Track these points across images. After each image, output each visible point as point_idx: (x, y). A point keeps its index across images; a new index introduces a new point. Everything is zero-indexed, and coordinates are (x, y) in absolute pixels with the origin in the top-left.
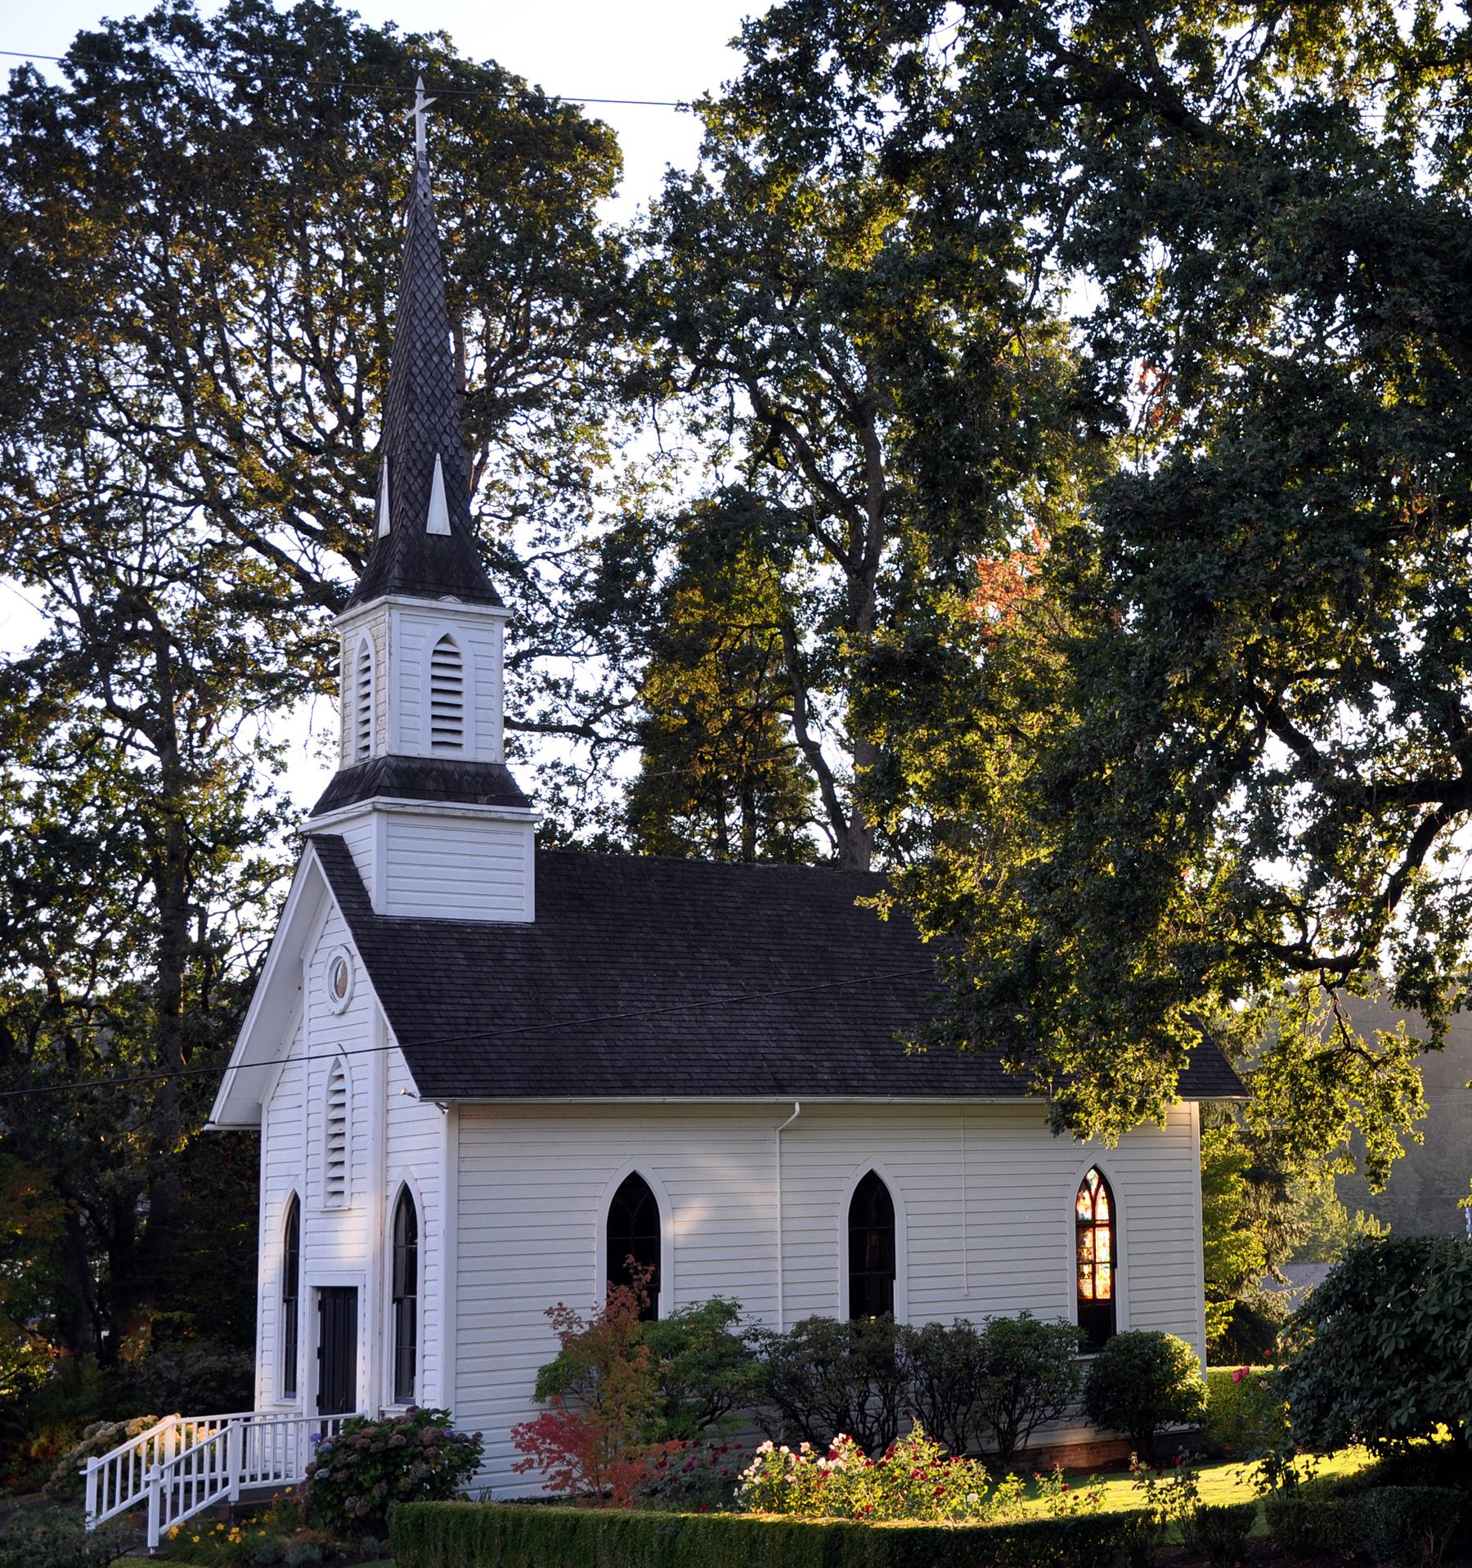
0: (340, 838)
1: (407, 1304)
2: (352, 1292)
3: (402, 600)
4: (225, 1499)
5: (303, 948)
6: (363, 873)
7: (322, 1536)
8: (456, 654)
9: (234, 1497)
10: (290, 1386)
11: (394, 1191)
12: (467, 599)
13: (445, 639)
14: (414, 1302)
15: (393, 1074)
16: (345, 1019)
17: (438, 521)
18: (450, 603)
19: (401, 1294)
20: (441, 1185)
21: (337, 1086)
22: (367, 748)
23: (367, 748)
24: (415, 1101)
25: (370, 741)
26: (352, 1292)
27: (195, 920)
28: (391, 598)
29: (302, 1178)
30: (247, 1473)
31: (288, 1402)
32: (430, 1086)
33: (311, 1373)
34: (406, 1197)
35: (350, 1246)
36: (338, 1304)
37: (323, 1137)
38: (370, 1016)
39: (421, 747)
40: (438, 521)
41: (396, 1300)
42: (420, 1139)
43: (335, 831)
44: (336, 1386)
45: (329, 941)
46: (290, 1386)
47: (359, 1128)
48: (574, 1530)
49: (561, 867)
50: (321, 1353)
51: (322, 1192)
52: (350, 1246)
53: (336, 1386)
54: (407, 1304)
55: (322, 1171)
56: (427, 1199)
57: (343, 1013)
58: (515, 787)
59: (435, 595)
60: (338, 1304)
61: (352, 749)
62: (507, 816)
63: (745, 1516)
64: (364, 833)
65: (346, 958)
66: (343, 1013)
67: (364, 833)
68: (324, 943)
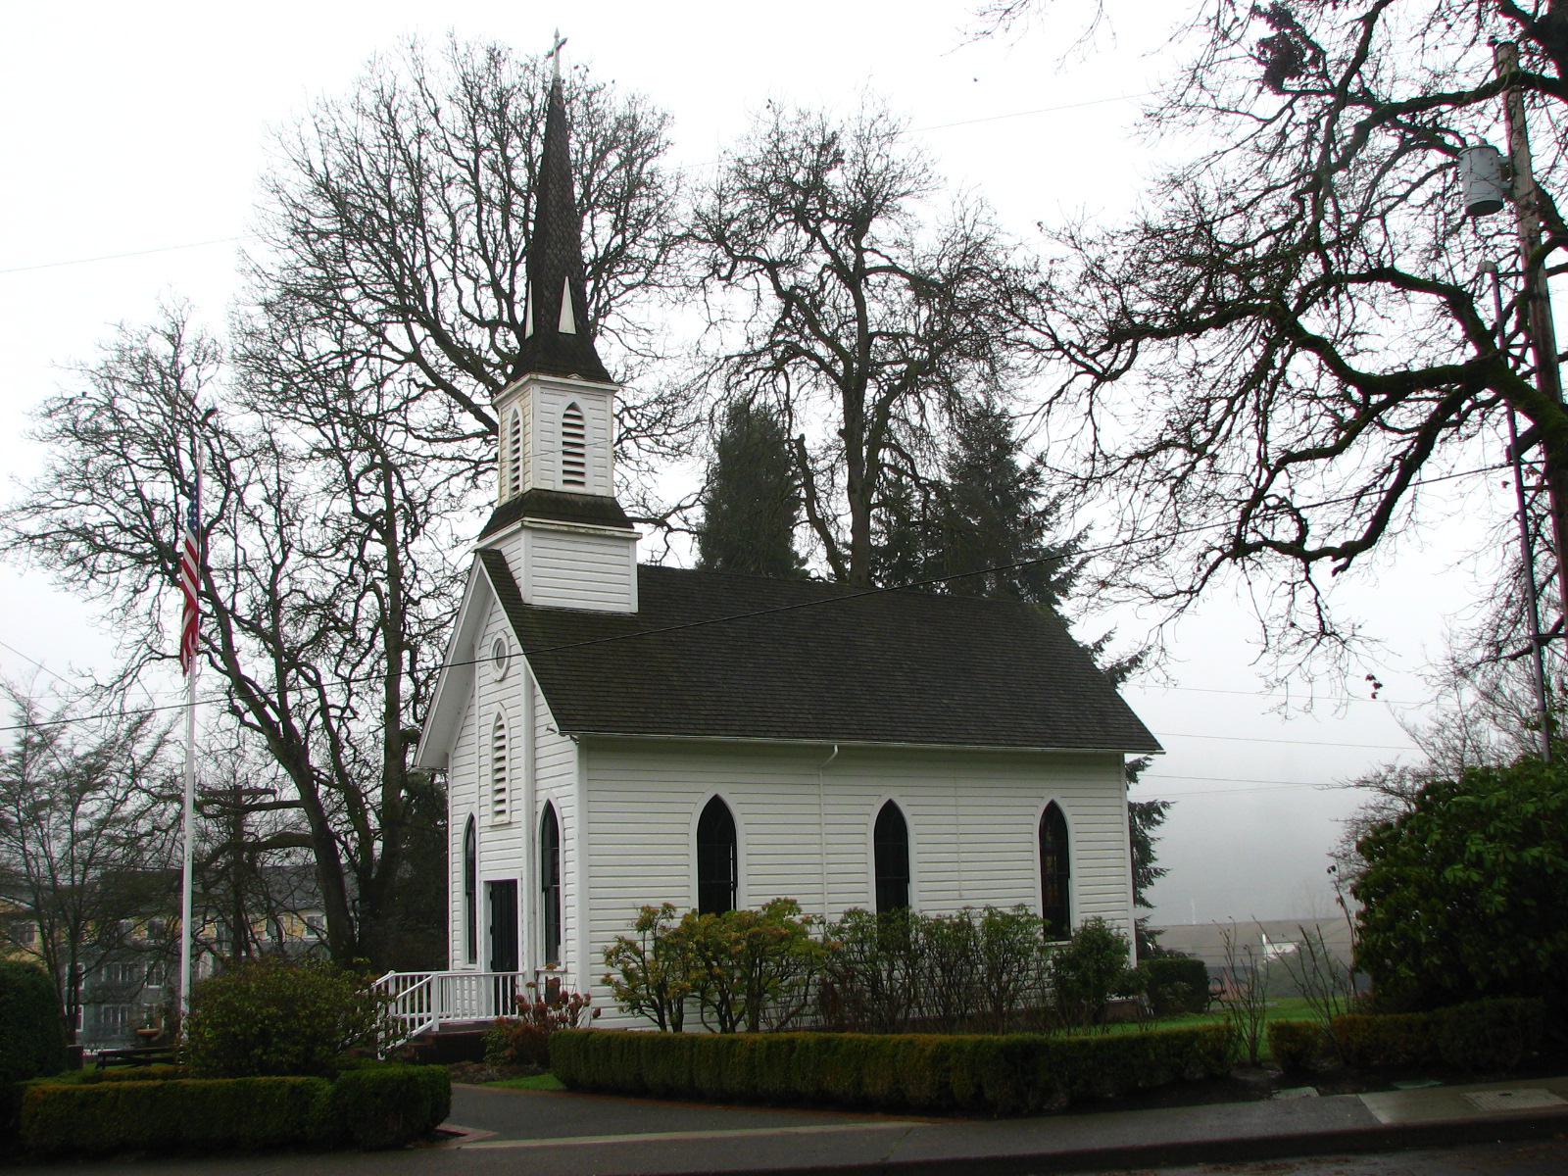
0: (499, 552)
1: (552, 891)
2: (514, 883)
3: (542, 377)
4: (430, 1028)
5: (472, 649)
6: (515, 575)
7: (1147, 831)
8: (579, 418)
9: (436, 1029)
10: (472, 956)
11: (541, 808)
12: (588, 378)
13: (572, 406)
14: (557, 890)
15: (540, 721)
16: (507, 683)
17: (567, 324)
18: (575, 380)
19: (547, 885)
20: (574, 800)
21: (500, 733)
22: (517, 487)
23: (517, 487)
24: (556, 737)
25: (520, 482)
26: (514, 883)
27: (406, 654)
28: (534, 376)
29: (476, 806)
30: (444, 1014)
31: (472, 966)
32: (566, 723)
33: (486, 945)
34: (549, 810)
35: (506, 856)
36: (504, 894)
37: (490, 782)
38: (521, 679)
39: (554, 482)
40: (567, 324)
41: (544, 889)
42: (557, 766)
43: (497, 548)
44: (505, 955)
45: (493, 628)
46: (472, 956)
47: (516, 763)
48: (792, 1050)
49: (652, 578)
50: (492, 930)
51: (490, 812)
52: (506, 856)
53: (505, 955)
54: (552, 891)
55: (489, 797)
56: (566, 812)
57: (502, 680)
58: (621, 511)
59: (566, 375)
60: (504, 894)
61: (507, 490)
62: (617, 534)
63: (979, 1037)
64: (521, 551)
65: (504, 639)
66: (502, 680)
67: (521, 551)
68: (488, 631)
